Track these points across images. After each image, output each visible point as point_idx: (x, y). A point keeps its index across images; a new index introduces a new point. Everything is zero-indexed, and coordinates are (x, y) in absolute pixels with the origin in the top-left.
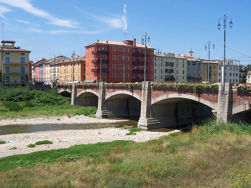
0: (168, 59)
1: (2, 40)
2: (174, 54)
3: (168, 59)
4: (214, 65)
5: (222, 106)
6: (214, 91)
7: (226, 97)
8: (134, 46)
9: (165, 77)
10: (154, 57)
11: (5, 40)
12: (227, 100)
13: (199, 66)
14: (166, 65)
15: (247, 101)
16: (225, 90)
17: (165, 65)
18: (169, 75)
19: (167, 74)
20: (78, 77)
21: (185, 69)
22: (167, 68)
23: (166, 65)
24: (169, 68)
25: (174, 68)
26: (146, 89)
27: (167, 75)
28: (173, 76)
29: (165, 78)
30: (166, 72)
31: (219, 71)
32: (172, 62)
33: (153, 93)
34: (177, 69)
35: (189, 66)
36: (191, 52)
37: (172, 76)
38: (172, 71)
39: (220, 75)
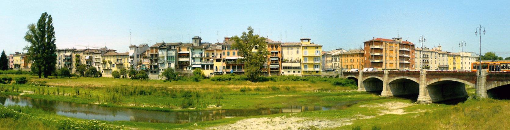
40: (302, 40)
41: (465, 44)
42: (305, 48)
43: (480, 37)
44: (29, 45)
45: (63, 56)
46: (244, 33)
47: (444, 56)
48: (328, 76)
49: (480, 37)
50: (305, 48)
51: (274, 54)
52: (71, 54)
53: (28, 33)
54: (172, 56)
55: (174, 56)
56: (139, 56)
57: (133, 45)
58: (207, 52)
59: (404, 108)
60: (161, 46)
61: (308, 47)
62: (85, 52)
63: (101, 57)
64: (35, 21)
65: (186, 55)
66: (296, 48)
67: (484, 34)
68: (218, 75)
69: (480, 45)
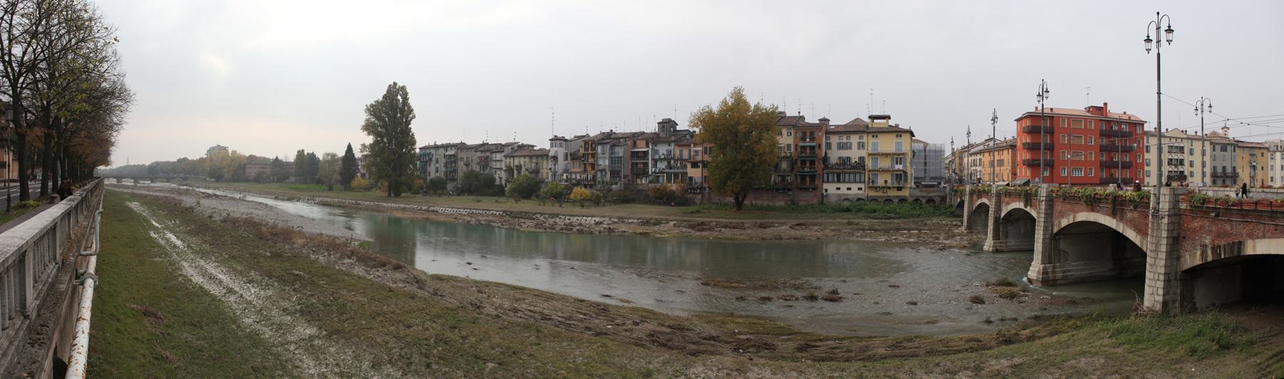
0: (1173, 140)
1: (870, 114)
2: (1186, 131)
3: (1173, 140)
4: (1262, 151)
5: (1154, 249)
6: (1142, 203)
7: (1163, 225)
8: (1104, 116)
9: (1167, 174)
10: (1145, 138)
11: (875, 113)
12: (1164, 234)
13: (1233, 153)
14: (1169, 152)
15: (1208, 237)
16: (1161, 206)
17: (1167, 152)
18: (1176, 169)
19: (1173, 168)
20: (1008, 175)
21: (1207, 159)
22: (1170, 157)
23: (1169, 152)
24: (1176, 157)
25: (1186, 157)
26: (1042, 198)
27: (1170, 169)
28: (1183, 172)
29: (1168, 176)
30: (1169, 164)
31: (1270, 163)
32: (1182, 145)
33: (1058, 207)
34: (1191, 158)
35: (1215, 153)
36: (1225, 127)
37: (1182, 172)
38: (1181, 162)
39: (1272, 169)
40: (873, 118)
41: (1210, 106)
42: (873, 137)
43: (1159, 54)
44: (369, 140)
45: (443, 156)
46: (725, 102)
47: (1226, 150)
48: (923, 197)
49: (1159, 54)
50: (873, 137)
51: (808, 151)
52: (457, 153)
53: (367, 120)
54: (618, 157)
55: (621, 157)
56: (569, 156)
57: (560, 135)
58: (680, 148)
59: (1007, 267)
60: (604, 139)
61: (879, 135)
62: (479, 149)
63: (503, 158)
64: (379, 94)
65: (642, 154)
66: (893, 136)
67: (1169, 41)
68: (694, 193)
69: (1159, 97)
